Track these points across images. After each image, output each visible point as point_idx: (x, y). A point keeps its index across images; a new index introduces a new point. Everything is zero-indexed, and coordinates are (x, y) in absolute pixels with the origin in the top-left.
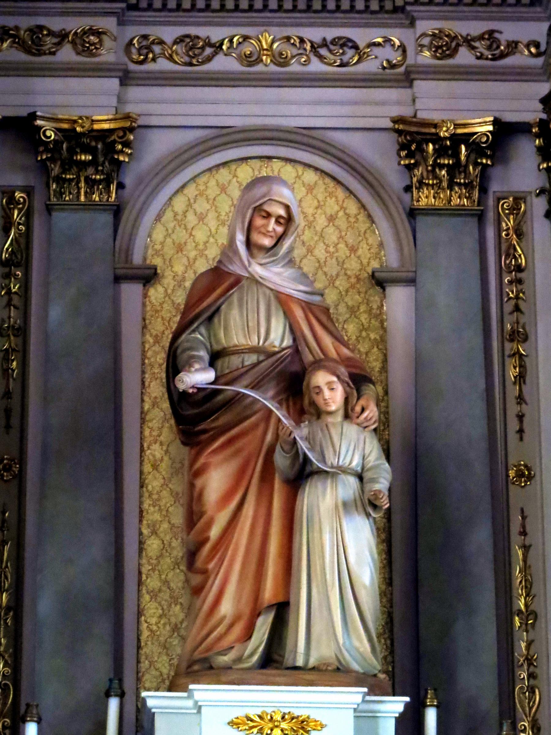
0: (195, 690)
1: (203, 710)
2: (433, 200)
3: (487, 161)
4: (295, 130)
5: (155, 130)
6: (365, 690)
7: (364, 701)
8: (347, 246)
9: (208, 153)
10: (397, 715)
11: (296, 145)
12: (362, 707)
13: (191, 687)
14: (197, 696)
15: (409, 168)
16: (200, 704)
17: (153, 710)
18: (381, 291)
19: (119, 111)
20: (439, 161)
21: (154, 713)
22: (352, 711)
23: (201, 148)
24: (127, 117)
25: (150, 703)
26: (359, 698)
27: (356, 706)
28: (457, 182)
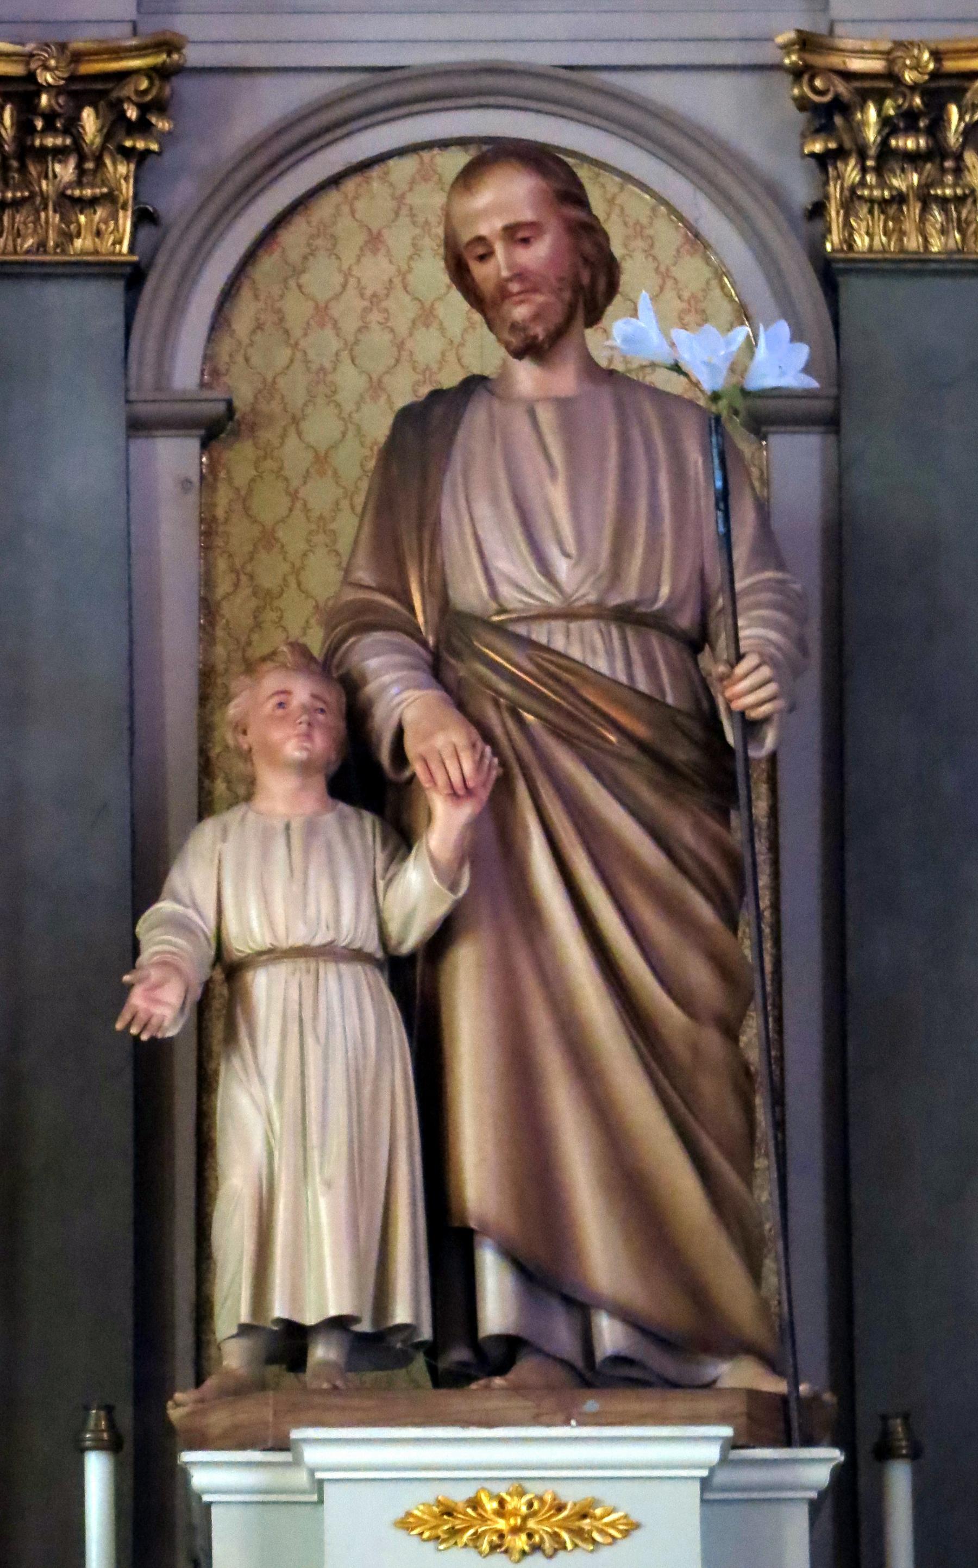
0: (305, 1441)
1: (328, 1489)
2: (884, 239)
3: (64, 140)
4: (552, 72)
5: (264, 81)
6: (727, 1431)
7: (724, 1461)
8: (442, 329)
9: (629, 134)
10: (813, 1495)
11: (381, 116)
12: (722, 1477)
13: (296, 1434)
14: (311, 1455)
15: (823, 161)
16: (319, 1475)
17: (206, 1498)
18: (477, 416)
19: (141, 28)
20: (893, 142)
21: (209, 1505)
22: (697, 1487)
23: (633, 116)
24: (169, 45)
25: (200, 1479)
26: (712, 1453)
27: (704, 1473)
28: (936, 196)
